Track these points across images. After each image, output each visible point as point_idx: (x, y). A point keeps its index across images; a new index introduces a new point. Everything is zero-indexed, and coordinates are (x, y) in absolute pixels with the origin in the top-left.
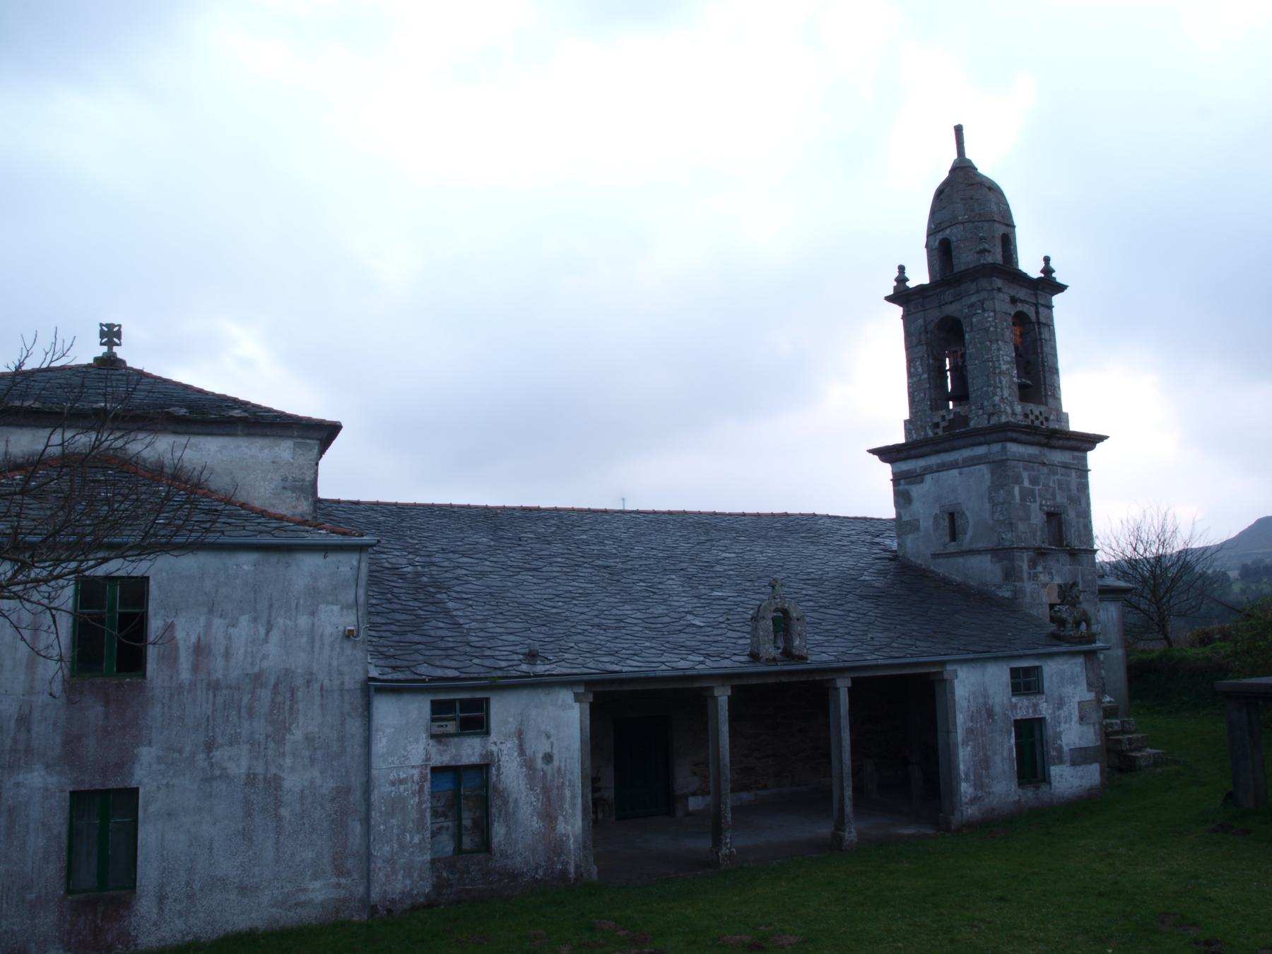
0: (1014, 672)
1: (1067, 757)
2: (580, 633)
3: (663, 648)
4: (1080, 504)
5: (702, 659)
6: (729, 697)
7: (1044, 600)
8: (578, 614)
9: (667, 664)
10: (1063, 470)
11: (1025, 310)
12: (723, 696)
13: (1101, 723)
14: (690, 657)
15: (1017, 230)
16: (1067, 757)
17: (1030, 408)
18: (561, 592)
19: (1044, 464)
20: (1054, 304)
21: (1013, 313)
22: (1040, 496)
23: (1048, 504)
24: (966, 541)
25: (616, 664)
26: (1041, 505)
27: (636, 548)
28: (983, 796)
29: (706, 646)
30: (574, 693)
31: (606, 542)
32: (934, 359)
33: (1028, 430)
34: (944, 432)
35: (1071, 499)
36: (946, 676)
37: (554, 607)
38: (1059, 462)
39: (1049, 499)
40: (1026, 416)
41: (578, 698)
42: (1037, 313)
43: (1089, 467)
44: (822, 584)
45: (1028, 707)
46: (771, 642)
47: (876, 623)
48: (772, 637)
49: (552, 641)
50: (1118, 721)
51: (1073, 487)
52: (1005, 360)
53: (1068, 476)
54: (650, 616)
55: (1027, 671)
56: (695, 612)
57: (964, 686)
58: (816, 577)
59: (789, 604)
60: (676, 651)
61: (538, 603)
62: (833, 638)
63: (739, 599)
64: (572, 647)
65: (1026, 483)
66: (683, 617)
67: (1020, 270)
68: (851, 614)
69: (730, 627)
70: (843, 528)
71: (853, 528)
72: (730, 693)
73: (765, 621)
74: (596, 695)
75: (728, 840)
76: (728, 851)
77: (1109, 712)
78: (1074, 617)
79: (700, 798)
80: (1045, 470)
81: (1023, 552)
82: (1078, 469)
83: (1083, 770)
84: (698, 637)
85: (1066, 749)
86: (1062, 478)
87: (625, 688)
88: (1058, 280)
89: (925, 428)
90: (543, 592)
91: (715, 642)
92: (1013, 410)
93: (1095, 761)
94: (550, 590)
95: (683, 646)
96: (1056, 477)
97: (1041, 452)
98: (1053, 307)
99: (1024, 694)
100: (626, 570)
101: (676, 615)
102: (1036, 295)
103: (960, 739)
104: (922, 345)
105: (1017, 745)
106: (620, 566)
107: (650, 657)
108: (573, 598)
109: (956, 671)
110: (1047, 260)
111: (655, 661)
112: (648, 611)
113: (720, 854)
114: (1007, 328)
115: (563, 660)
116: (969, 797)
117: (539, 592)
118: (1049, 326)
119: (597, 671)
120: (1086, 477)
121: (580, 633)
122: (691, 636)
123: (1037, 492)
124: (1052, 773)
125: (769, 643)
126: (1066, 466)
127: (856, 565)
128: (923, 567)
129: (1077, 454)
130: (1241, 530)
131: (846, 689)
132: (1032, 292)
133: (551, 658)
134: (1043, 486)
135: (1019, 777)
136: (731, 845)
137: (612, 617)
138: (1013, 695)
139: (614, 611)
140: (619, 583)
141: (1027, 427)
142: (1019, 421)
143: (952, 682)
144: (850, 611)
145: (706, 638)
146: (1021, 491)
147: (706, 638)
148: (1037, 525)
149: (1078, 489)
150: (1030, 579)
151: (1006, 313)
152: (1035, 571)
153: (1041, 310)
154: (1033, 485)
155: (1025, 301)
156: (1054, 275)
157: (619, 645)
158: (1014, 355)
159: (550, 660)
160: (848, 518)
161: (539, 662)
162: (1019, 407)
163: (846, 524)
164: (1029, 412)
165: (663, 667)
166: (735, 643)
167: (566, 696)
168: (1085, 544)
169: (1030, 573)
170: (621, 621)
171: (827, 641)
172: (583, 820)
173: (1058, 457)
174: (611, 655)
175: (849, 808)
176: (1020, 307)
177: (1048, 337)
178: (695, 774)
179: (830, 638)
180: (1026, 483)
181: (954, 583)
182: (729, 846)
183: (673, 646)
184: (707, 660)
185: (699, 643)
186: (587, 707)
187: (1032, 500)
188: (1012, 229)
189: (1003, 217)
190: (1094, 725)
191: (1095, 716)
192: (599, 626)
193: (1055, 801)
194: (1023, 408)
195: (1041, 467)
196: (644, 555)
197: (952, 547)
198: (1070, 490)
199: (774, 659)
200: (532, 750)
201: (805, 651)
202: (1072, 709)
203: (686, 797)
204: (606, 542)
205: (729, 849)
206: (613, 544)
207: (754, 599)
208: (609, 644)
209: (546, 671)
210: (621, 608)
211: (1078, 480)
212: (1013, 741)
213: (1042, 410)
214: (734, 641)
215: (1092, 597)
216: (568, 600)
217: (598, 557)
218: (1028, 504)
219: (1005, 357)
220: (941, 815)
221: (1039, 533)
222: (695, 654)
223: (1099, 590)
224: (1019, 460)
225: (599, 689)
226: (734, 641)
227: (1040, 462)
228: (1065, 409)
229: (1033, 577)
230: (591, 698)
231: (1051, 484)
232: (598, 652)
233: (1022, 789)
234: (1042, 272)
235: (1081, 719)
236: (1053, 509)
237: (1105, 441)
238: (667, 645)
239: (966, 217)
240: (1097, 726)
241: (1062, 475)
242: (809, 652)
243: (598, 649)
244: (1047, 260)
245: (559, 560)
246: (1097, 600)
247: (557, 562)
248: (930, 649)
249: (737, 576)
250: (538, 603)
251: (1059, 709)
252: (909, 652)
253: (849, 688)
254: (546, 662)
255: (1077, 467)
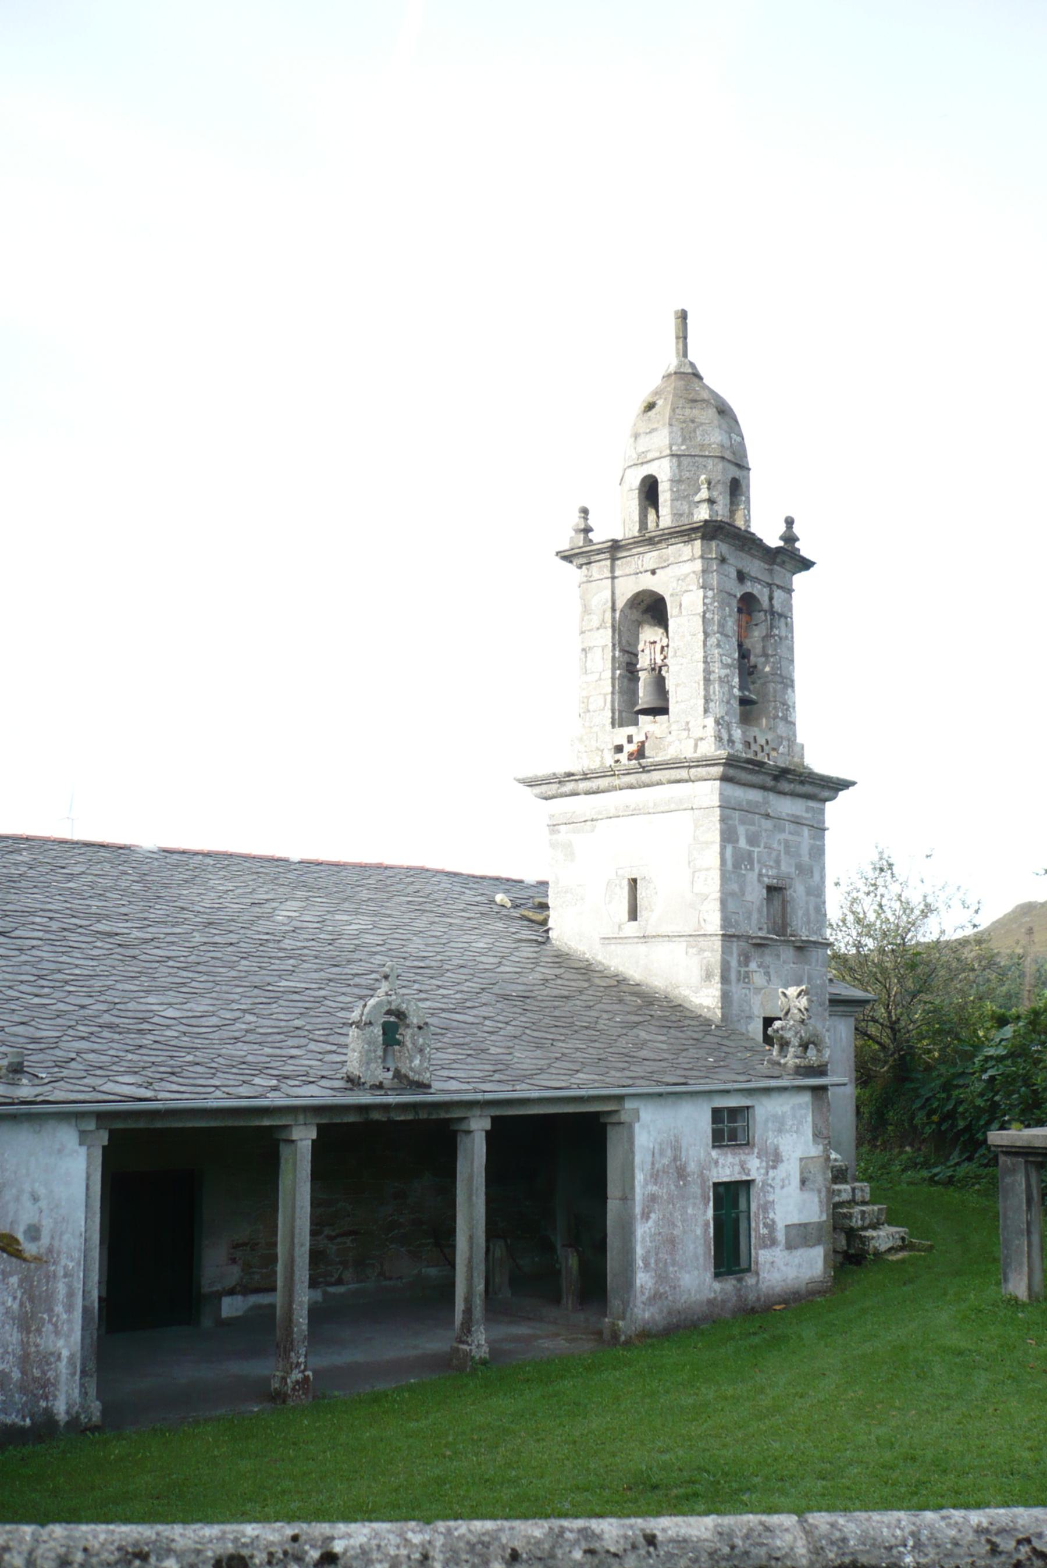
0: (717, 1114)
1: (781, 1236)
2: (83, 1038)
3: (214, 1065)
4: (812, 877)
5: (274, 1082)
6: (313, 1141)
7: (756, 1013)
8: (77, 1008)
9: (224, 1089)
10: (793, 826)
11: (755, 592)
12: (304, 1136)
13: (828, 1190)
14: (257, 1080)
15: (753, 475)
16: (781, 1236)
17: (753, 734)
18: (45, 972)
19: (767, 816)
20: (794, 587)
21: (739, 596)
22: (759, 862)
23: (770, 873)
24: (651, 918)
25: (146, 1088)
26: (760, 875)
27: (159, 907)
28: (666, 1292)
29: (279, 1064)
30: (79, 1131)
31: (108, 894)
32: (623, 651)
33: (750, 766)
34: (629, 759)
35: (799, 867)
36: (624, 1117)
37: (37, 996)
38: (788, 815)
39: (771, 867)
40: (748, 744)
41: (84, 1137)
42: (771, 599)
43: (827, 825)
44: (442, 975)
45: (733, 1165)
46: (380, 1061)
47: (524, 1037)
48: (380, 1053)
49: (41, 1050)
50: (848, 1187)
51: (805, 850)
52: (725, 662)
53: (799, 835)
54: (190, 1014)
55: (734, 1113)
56: (255, 1011)
57: (649, 1132)
58: (433, 964)
59: (407, 1005)
60: (234, 1070)
61: (10, 987)
62: (464, 1057)
63: (322, 993)
64: (73, 1059)
65: (743, 843)
66: (240, 1018)
67: (753, 534)
68: (487, 1022)
69: (311, 1036)
70: (467, 891)
71: (481, 891)
72: (314, 1136)
73: (371, 1028)
74: (112, 1133)
75: (302, 1360)
76: (300, 1375)
77: (839, 1175)
78: (801, 1038)
79: (240, 1298)
80: (768, 824)
81: (732, 942)
82: (812, 826)
83: (800, 1256)
84: (266, 1049)
85: (780, 1226)
86: (790, 837)
87: (159, 1124)
88: (803, 553)
89: (602, 751)
90: (16, 970)
91: (292, 1057)
92: (730, 735)
93: (818, 1242)
94: (28, 968)
95: (244, 1063)
96: (783, 836)
97: (764, 798)
98: (794, 590)
99: (727, 1146)
100: (146, 941)
101: (229, 1015)
102: (771, 571)
103: (638, 1210)
104: (606, 628)
105: (716, 1218)
106: (136, 934)
107: (195, 1078)
108: (66, 982)
109: (637, 1111)
110: (790, 522)
111: (204, 1084)
112: (185, 1007)
113: (289, 1381)
114: (730, 616)
115: (62, 1079)
116: (647, 1294)
117: (9, 969)
118: (786, 617)
119: (119, 1098)
120: (823, 838)
121: (83, 1038)
122: (256, 1047)
123: (756, 854)
124: (761, 1259)
125: (377, 1062)
126: (797, 821)
127: (490, 949)
128: (586, 956)
129: (812, 804)
130: (995, 919)
131: (484, 1134)
132: (767, 567)
133: (44, 1075)
134: (765, 848)
135: (717, 1266)
136: (305, 1366)
137: (129, 1014)
138: (714, 1147)
139: (132, 1006)
140: (135, 961)
141: (749, 761)
142: (737, 751)
143: (630, 1127)
144: (485, 1018)
145: (278, 1052)
146: (734, 855)
147: (278, 1052)
148: (752, 902)
149: (810, 854)
150: (739, 980)
151: (730, 594)
152: (747, 969)
153: (778, 594)
154: (752, 845)
155: (757, 578)
156: (797, 545)
157: (146, 1058)
158: (736, 655)
159: (42, 1078)
160: (474, 877)
161: (25, 1081)
162: (739, 731)
163: (471, 885)
164: (752, 740)
165: (218, 1094)
166: (320, 1060)
167: (67, 1136)
168: (816, 933)
169: (739, 972)
170: (144, 1020)
171: (455, 1061)
172: (83, 1329)
173: (787, 807)
174: (136, 1073)
175: (478, 1312)
176: (749, 587)
177: (783, 634)
178: (234, 1261)
179: (460, 1057)
180: (743, 843)
181: (632, 983)
182: (302, 1367)
183: (229, 1062)
184: (281, 1084)
185: (268, 1059)
186: (98, 1154)
187: (748, 867)
188: (745, 473)
189: (734, 453)
190: (819, 1191)
191: (821, 1179)
192: (110, 1026)
193: (763, 1299)
194: (743, 733)
195: (763, 821)
196: (170, 919)
197: (632, 929)
198: (800, 856)
199: (380, 1086)
200: (10, 1220)
201: (428, 1075)
202: (790, 1169)
203: (219, 1295)
204: (108, 894)
205: (303, 1372)
206: (121, 899)
207: (343, 994)
208: (130, 1056)
209: (37, 1096)
210: (142, 1000)
211: (812, 841)
212: (710, 1213)
213: (769, 739)
214: (320, 1057)
215: (820, 1008)
216: (58, 984)
217: (100, 918)
218: (743, 872)
219: (724, 658)
220: (607, 1320)
221: (755, 916)
222: (262, 1076)
223: (831, 1001)
224: (734, 809)
225: (119, 1125)
226: (320, 1057)
227: (763, 812)
228: (799, 740)
229: (744, 978)
230: (104, 1138)
231: (775, 846)
232: (115, 1068)
233: (719, 1282)
234: (782, 538)
235: (803, 1182)
236: (775, 881)
237: (850, 788)
238: (220, 1060)
239: (683, 447)
240: (823, 1194)
241: (790, 833)
242: (433, 1077)
243: (114, 1063)
244: (790, 522)
245: (38, 920)
246: (827, 1014)
247: (33, 923)
248: (602, 1078)
249: (316, 958)
250: (10, 987)
251: (774, 1167)
252: (573, 1081)
253: (487, 1132)
254: (36, 1081)
255: (811, 824)
